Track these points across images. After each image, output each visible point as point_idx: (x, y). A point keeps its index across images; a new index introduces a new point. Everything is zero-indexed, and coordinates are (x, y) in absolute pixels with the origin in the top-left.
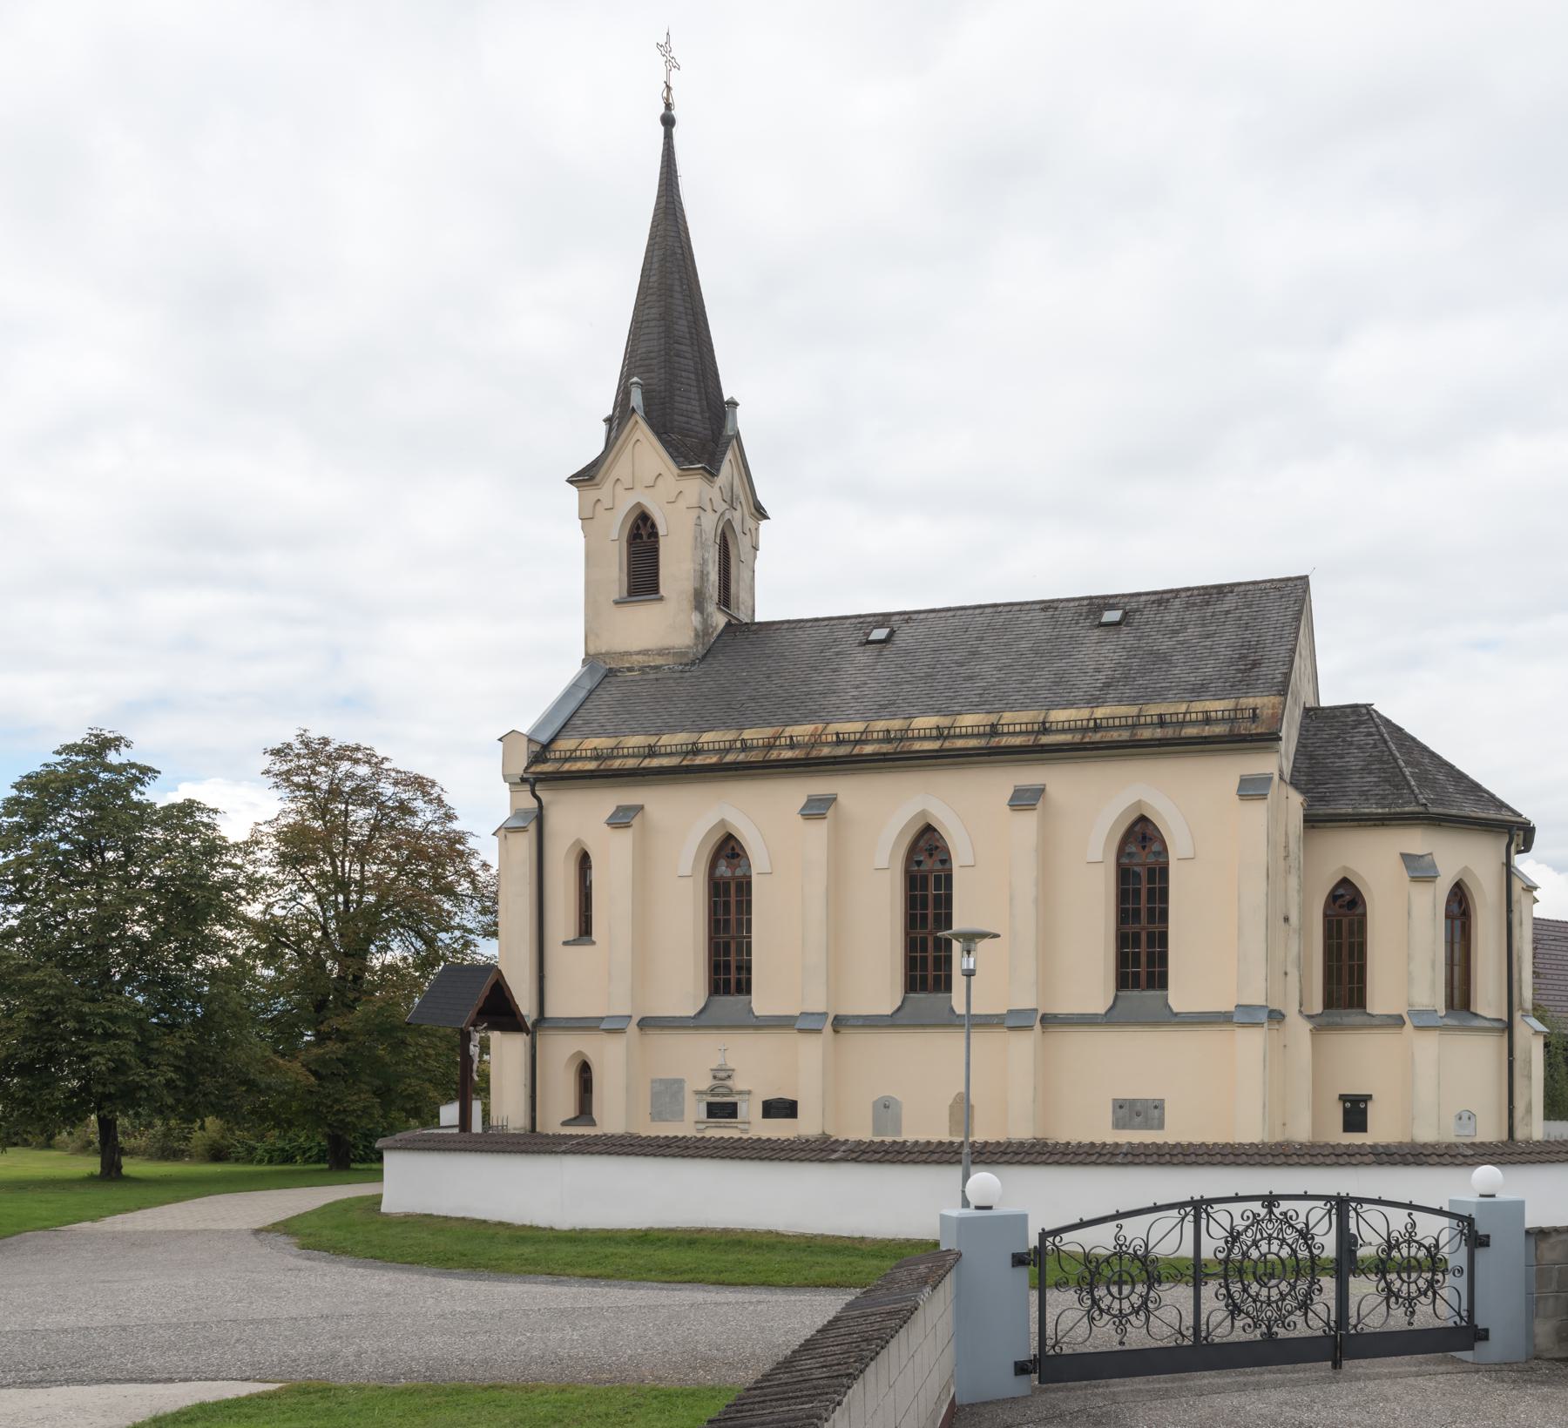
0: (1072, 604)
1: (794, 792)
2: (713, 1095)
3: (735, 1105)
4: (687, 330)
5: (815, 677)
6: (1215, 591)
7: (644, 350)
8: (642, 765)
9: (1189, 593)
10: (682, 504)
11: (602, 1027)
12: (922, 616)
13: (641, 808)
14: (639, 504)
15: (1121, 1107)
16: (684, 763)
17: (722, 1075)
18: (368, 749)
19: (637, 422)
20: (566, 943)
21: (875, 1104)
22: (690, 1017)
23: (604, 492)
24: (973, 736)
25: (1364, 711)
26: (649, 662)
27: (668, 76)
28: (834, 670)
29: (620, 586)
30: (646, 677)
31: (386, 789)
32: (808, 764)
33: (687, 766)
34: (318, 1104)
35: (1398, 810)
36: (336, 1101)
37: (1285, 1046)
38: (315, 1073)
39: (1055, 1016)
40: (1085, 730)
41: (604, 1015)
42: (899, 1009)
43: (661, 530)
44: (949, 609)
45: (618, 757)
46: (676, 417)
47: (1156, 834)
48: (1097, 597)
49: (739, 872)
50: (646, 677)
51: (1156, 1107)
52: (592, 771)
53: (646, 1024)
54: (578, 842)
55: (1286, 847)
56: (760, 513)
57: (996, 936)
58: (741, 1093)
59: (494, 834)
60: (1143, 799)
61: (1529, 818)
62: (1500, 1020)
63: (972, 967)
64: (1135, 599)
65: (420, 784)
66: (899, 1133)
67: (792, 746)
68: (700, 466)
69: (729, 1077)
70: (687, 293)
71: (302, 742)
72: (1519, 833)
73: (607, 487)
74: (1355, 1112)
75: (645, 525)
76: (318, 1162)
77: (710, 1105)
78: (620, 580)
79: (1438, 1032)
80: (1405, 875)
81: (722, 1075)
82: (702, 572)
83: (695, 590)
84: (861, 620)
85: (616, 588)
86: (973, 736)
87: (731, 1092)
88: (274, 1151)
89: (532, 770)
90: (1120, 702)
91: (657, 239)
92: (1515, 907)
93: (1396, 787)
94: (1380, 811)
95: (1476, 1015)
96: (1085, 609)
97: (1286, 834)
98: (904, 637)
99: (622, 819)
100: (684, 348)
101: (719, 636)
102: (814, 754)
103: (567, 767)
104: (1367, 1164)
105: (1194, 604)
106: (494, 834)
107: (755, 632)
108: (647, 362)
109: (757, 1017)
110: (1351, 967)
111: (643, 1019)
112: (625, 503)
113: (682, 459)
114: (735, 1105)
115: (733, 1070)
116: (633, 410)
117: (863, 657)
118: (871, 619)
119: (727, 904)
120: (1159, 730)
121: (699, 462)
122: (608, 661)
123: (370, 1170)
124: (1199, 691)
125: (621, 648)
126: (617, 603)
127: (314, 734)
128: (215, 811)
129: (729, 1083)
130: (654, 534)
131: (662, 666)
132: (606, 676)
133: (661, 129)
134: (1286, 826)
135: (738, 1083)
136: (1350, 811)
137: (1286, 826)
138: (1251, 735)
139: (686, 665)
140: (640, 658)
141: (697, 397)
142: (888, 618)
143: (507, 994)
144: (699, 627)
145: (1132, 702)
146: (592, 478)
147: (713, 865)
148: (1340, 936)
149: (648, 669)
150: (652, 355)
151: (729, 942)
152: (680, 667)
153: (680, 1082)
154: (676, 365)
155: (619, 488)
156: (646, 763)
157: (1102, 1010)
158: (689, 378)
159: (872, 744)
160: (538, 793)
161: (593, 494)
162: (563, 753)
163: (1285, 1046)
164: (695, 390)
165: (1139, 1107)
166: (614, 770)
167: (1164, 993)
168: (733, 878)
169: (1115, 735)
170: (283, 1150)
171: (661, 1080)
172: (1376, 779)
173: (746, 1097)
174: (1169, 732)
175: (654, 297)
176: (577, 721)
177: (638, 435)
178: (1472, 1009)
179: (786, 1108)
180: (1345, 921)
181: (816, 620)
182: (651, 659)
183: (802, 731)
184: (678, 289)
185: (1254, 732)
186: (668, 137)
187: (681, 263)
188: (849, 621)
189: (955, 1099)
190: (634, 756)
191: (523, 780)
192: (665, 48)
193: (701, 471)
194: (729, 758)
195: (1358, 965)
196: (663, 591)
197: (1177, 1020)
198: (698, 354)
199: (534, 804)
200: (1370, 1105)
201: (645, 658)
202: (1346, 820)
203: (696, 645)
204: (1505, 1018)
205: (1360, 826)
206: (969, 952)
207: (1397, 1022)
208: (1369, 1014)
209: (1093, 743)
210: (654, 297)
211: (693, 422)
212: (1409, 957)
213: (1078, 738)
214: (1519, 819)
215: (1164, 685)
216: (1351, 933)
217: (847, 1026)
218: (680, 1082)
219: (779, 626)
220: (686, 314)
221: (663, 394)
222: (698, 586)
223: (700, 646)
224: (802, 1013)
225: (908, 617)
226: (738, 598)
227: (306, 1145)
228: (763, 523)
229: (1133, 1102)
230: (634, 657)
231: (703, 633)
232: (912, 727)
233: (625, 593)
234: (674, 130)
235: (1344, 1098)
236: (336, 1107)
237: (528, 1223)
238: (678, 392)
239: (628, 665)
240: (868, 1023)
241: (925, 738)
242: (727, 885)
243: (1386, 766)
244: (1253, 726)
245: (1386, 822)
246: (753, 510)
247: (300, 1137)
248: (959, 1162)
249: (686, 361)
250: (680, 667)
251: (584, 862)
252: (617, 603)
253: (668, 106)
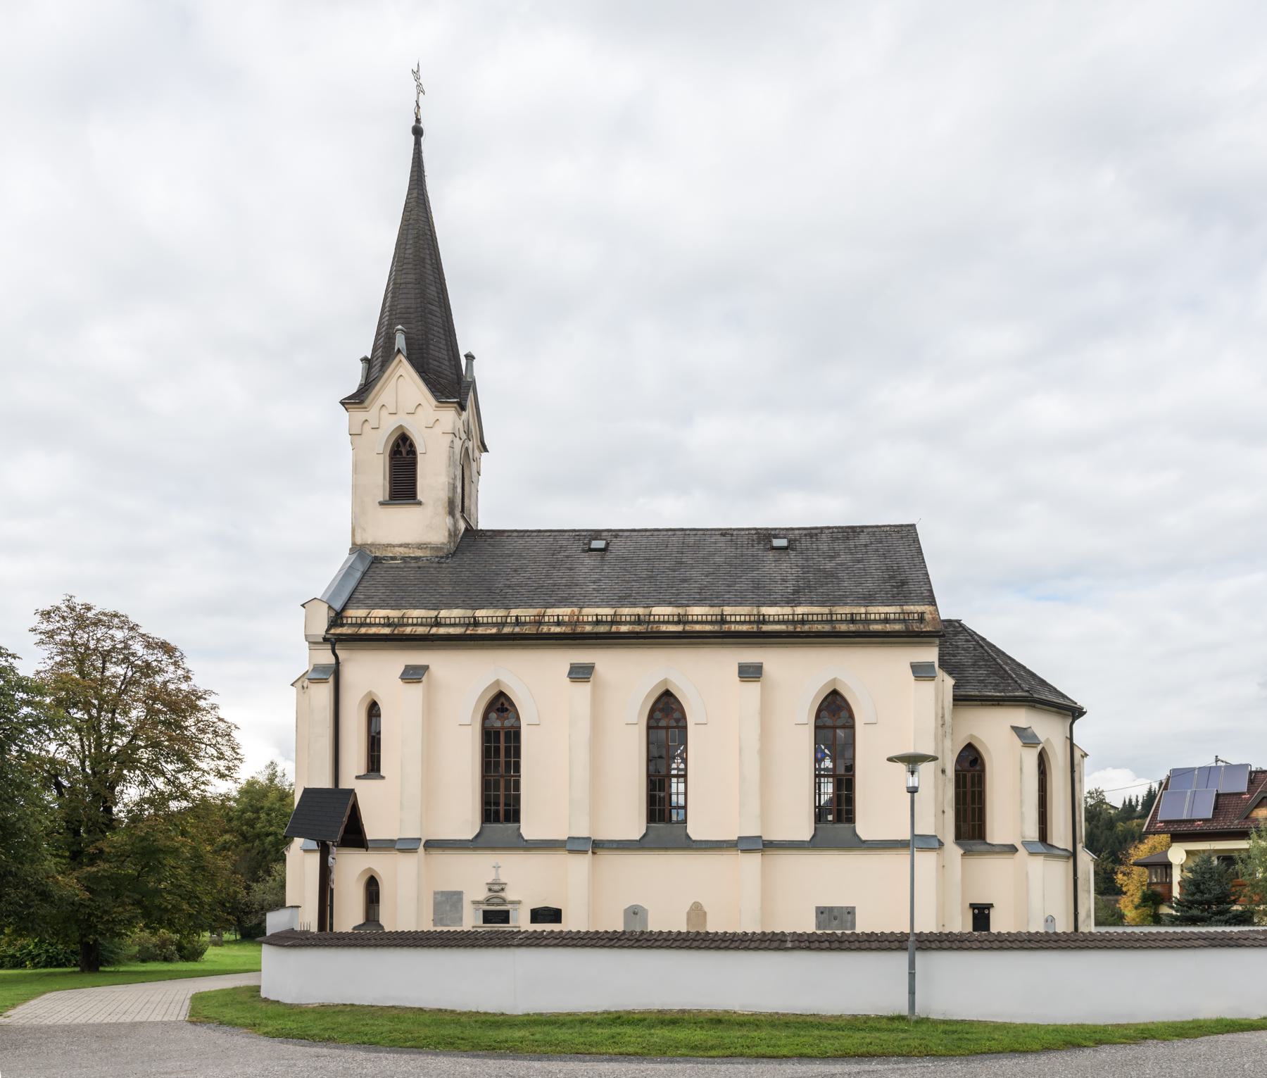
0: (743, 533)
1: (560, 660)
2: (489, 905)
3: (507, 912)
4: (436, 295)
5: (555, 573)
6: (850, 530)
7: (403, 306)
8: (431, 632)
9: (831, 531)
10: (438, 429)
11: (396, 847)
12: (626, 534)
13: (426, 668)
14: (401, 427)
15: (822, 913)
16: (468, 632)
17: (496, 888)
18: (123, 616)
19: (401, 360)
20: (358, 777)
21: (626, 911)
22: (469, 840)
23: (372, 412)
24: (707, 622)
25: (957, 625)
26: (410, 553)
27: (418, 98)
28: (570, 569)
29: (384, 490)
30: (408, 565)
31: (138, 647)
32: (573, 638)
33: (471, 635)
34: (90, 915)
35: (1011, 694)
36: (105, 912)
37: (943, 866)
38: (88, 889)
39: (771, 842)
40: (793, 622)
41: (395, 838)
42: (645, 836)
43: (419, 449)
44: (646, 530)
45: (408, 625)
46: (431, 361)
47: (843, 704)
48: (761, 529)
49: (507, 723)
50: (408, 565)
51: (849, 913)
52: (386, 635)
53: (432, 845)
54: (370, 693)
55: (943, 717)
56: (484, 448)
57: (890, 759)
58: (513, 903)
59: (292, 685)
60: (668, 678)
61: (1082, 705)
62: (1066, 850)
63: (916, 785)
64: (791, 532)
65: (167, 649)
66: (853, 926)
67: (558, 623)
68: (456, 400)
69: (503, 889)
70: (435, 266)
71: (67, 606)
72: (1075, 712)
73: (374, 409)
74: (981, 915)
75: (404, 443)
76: (45, 967)
77: (485, 912)
78: (384, 485)
79: (1042, 857)
80: (1018, 742)
81: (496, 888)
82: (454, 484)
83: (449, 498)
84: (577, 533)
85: (381, 493)
86: (707, 622)
87: (504, 902)
88: (5, 957)
89: (332, 631)
90: (812, 604)
91: (411, 221)
92: (1076, 769)
93: (1002, 678)
94: (998, 694)
95: (1052, 846)
96: (755, 537)
97: (943, 708)
98: (617, 545)
99: (413, 675)
100: (434, 308)
101: (462, 538)
102: (579, 630)
103: (363, 630)
104: (1117, 948)
105: (838, 539)
106: (292, 685)
107: (491, 537)
108: (405, 316)
109: (526, 841)
110: (974, 809)
111: (427, 842)
112: (389, 426)
113: (439, 394)
114: (507, 912)
115: (506, 884)
116: (399, 351)
117: (589, 561)
118: (585, 533)
119: (497, 749)
120: (852, 625)
121: (455, 398)
122: (373, 550)
123: (118, 972)
124: (869, 599)
125: (385, 541)
126: (381, 504)
127: (79, 600)
128: (14, 657)
129: (502, 894)
130: (412, 452)
131: (421, 557)
132: (373, 563)
133: (413, 138)
134: (943, 702)
135: (510, 895)
136: (977, 693)
137: (943, 702)
138: (922, 632)
139: (442, 557)
140: (402, 550)
141: (445, 347)
142: (599, 533)
143: (358, 814)
144: (452, 529)
145: (822, 604)
146: (362, 402)
147: (485, 717)
148: (965, 786)
149: (408, 560)
150: (411, 310)
151: (499, 780)
152: (437, 560)
153: (459, 895)
154: (430, 321)
155: (384, 413)
156: (434, 630)
157: (807, 838)
158: (438, 332)
159: (625, 625)
160: (337, 651)
161: (360, 415)
162: (354, 619)
163: (943, 866)
164: (444, 342)
165: (836, 913)
166: (406, 635)
167: (853, 825)
168: (503, 728)
169: (819, 627)
170: (13, 956)
171: (442, 892)
172: (985, 672)
173: (517, 906)
174: (861, 627)
175: (410, 266)
176: (357, 595)
177: (401, 371)
178: (1049, 842)
179: (551, 915)
180: (969, 775)
181: (539, 531)
182: (411, 551)
183: (564, 612)
184: (429, 262)
185: (924, 630)
186: (418, 144)
187: (431, 243)
188: (567, 534)
189: (691, 907)
190: (422, 625)
191: (325, 640)
192: (416, 74)
193: (456, 405)
194: (507, 630)
195: (978, 808)
196: (419, 497)
197: (865, 846)
198: (444, 315)
199: (332, 660)
200: (992, 910)
201: (406, 550)
202: (976, 700)
203: (449, 542)
204: (1070, 848)
205: (982, 705)
206: (913, 773)
207: (1012, 849)
208: (989, 844)
209: (802, 632)
210: (410, 266)
211: (443, 367)
212: (1022, 802)
213: (791, 628)
214: (1075, 706)
215: (840, 593)
216: (973, 784)
217: (602, 848)
218: (459, 895)
219: (509, 534)
220: (435, 283)
221: (421, 342)
222: (451, 495)
223: (452, 544)
224: (569, 838)
225: (616, 533)
226: (470, 510)
227: (35, 952)
228: (484, 454)
229: (831, 909)
230: (397, 549)
231: (453, 534)
232: (653, 613)
233: (387, 498)
234: (422, 139)
235: (973, 906)
236: (106, 918)
237: (474, 1010)
238: (432, 342)
239: (391, 555)
240: (621, 846)
241: (668, 622)
242: (497, 734)
243: (989, 663)
244: (922, 626)
245: (1001, 703)
246: (479, 443)
247: (30, 946)
248: (906, 949)
249: (436, 319)
250: (437, 560)
251: (373, 711)
252: (381, 504)
253: (418, 120)
